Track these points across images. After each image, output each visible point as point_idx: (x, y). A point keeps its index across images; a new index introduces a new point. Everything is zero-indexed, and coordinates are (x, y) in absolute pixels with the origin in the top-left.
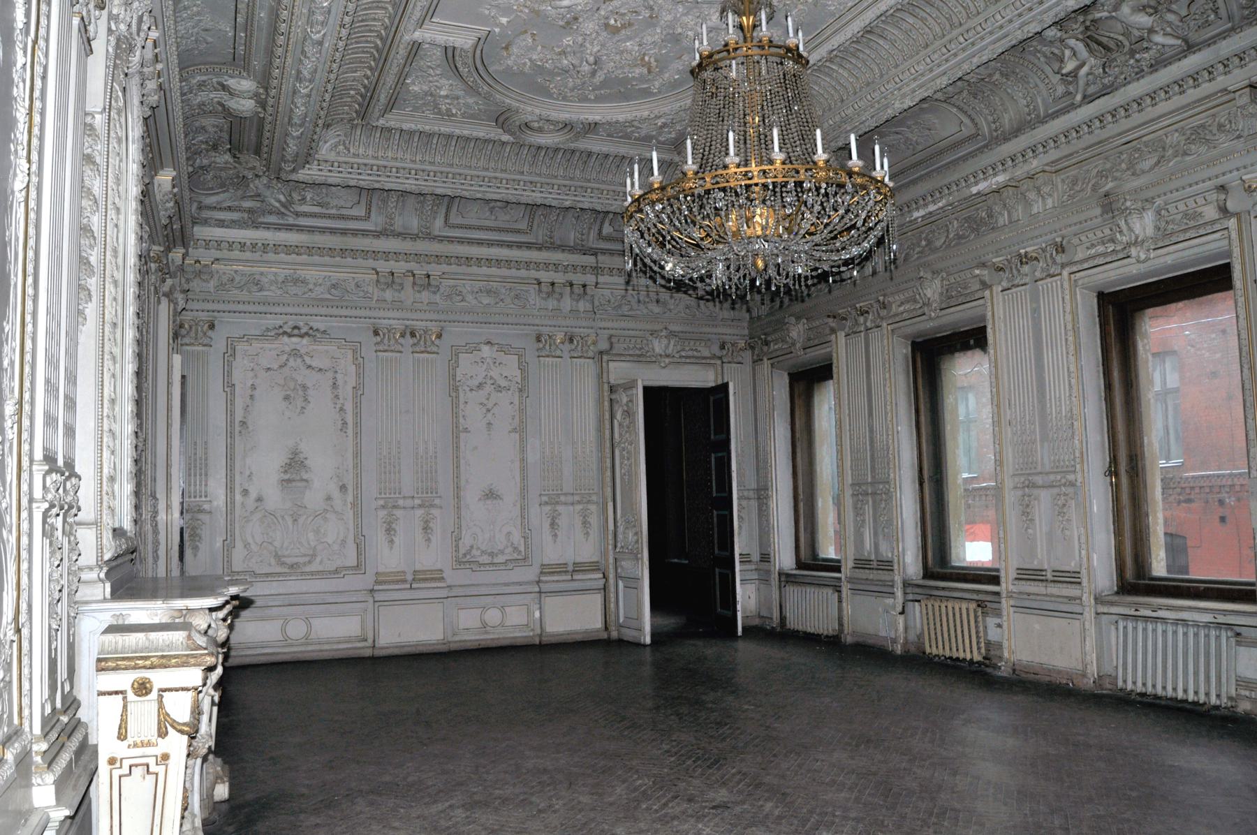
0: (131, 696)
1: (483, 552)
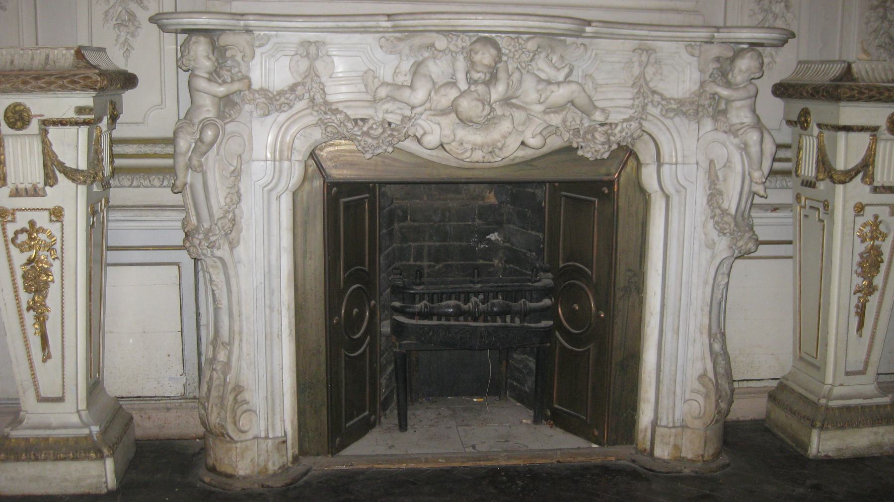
0: (884, 133)
1: (483, 109)
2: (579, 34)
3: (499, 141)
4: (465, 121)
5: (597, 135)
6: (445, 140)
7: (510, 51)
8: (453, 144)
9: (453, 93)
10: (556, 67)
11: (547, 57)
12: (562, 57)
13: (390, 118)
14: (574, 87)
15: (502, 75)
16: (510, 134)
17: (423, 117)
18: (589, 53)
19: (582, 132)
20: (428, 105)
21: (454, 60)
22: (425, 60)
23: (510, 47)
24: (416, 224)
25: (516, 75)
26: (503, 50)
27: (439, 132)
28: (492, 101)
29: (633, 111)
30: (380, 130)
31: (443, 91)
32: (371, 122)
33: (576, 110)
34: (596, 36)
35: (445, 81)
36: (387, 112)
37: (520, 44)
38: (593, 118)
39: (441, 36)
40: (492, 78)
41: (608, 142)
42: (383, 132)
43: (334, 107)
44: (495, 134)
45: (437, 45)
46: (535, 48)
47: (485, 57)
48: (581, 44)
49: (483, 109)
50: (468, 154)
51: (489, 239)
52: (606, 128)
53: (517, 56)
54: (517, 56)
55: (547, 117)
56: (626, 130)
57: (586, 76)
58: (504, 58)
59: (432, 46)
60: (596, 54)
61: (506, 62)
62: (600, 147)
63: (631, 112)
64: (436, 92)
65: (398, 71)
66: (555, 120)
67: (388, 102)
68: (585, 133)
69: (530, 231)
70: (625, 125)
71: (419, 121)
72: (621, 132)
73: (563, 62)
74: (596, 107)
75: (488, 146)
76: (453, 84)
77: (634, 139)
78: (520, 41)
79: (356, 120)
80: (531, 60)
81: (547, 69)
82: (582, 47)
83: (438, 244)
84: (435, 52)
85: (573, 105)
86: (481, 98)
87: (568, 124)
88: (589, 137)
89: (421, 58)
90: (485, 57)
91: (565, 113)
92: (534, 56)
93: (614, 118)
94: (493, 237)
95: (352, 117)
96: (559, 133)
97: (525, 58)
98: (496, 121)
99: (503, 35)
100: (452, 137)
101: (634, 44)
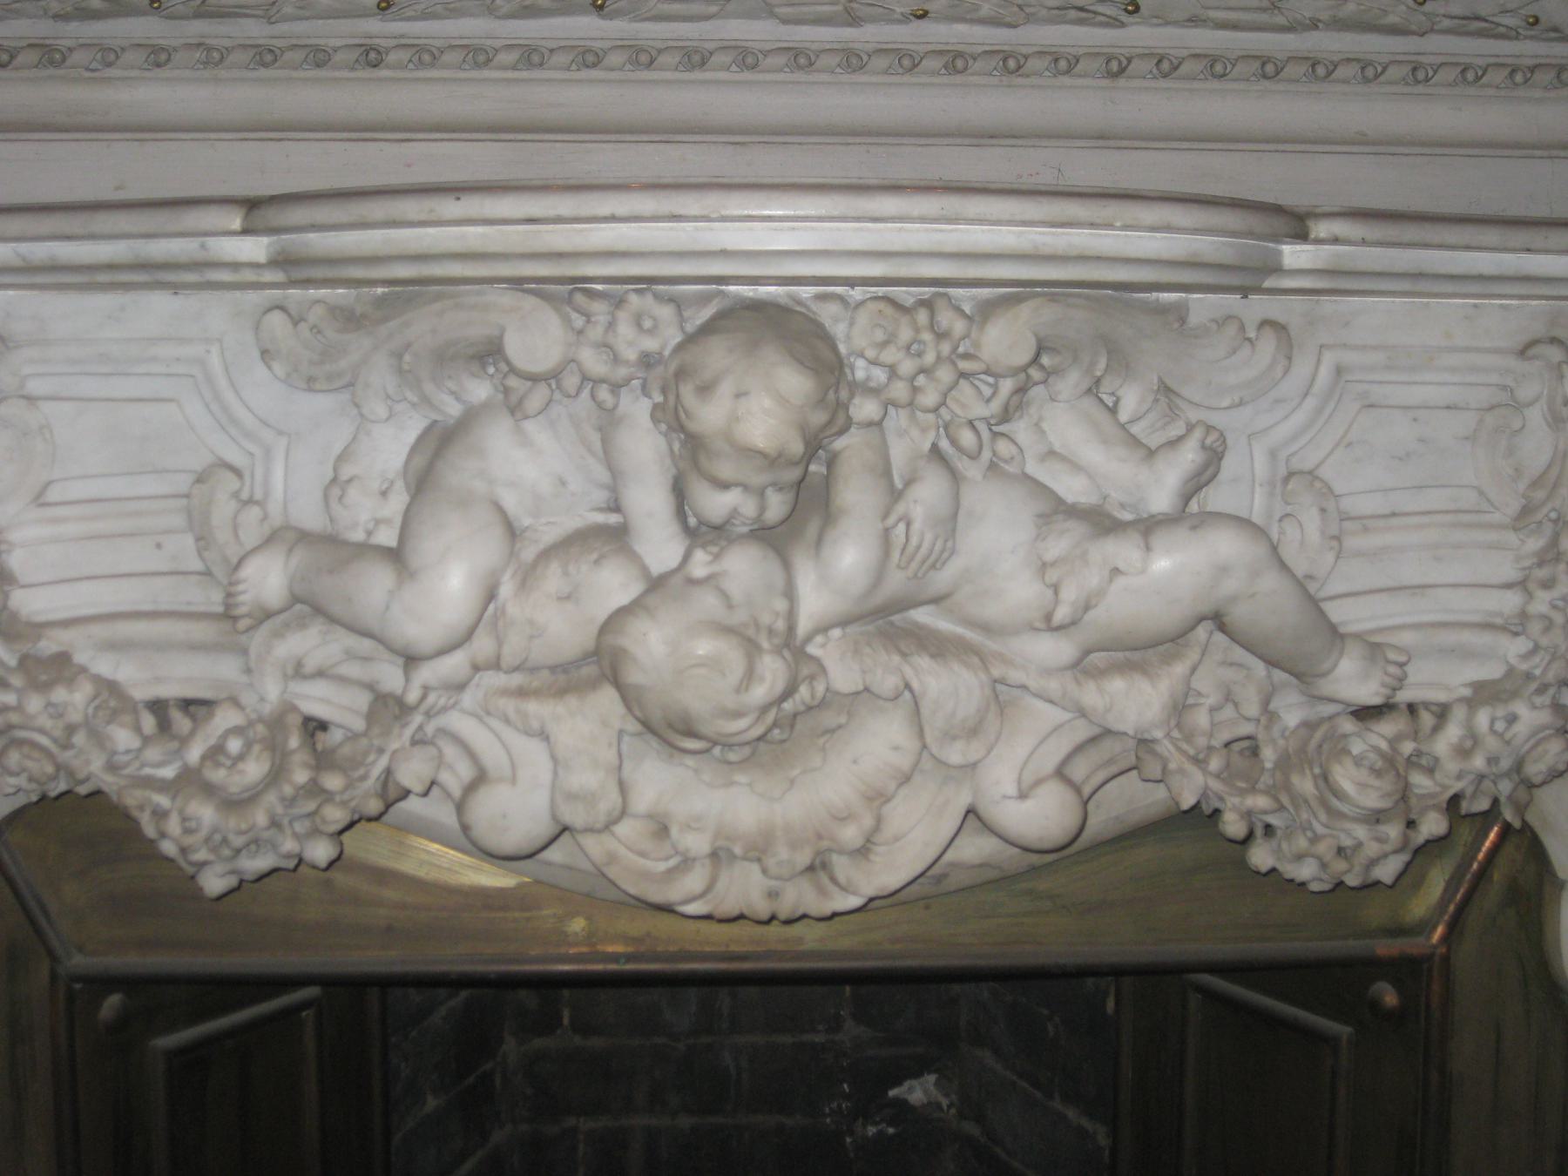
1: (750, 676)
2: (1251, 277)
3: (844, 818)
4: (671, 731)
5: (1346, 777)
6: (575, 815)
7: (892, 371)
8: (624, 829)
9: (613, 586)
10: (1135, 442)
11: (1093, 390)
12: (1166, 389)
13: (317, 699)
14: (1226, 545)
15: (856, 495)
16: (906, 779)
17: (468, 699)
18: (1302, 368)
19: (1269, 755)
20: (483, 645)
21: (609, 422)
22: (471, 417)
23: (890, 355)
24: (596, 1042)
25: (929, 494)
26: (861, 370)
27: (545, 776)
28: (804, 625)
29: (1520, 645)
30: (254, 769)
31: (553, 579)
32: (225, 719)
33: (1239, 654)
34: (1339, 281)
35: (571, 523)
36: (298, 671)
37: (941, 336)
38: (1327, 687)
39: (530, 302)
40: (804, 501)
41: (1404, 808)
42: (276, 775)
43: (48, 646)
44: (827, 786)
45: (514, 346)
46: (1023, 356)
47: (759, 406)
48: (1265, 323)
49: (750, 676)
50: (694, 881)
51: (901, 1104)
52: (1388, 727)
53: (929, 398)
54: (929, 398)
55: (1091, 695)
56: (1492, 743)
57: (1293, 478)
58: (865, 409)
59: (489, 353)
60: (1339, 371)
61: (878, 424)
62: (1361, 832)
63: (1514, 648)
64: (527, 578)
65: (347, 471)
66: (1136, 702)
67: (301, 623)
68: (1285, 764)
69: (1057, 1104)
70: (1482, 719)
71: (458, 722)
72: (1463, 752)
73: (1172, 413)
74: (1336, 636)
75: (794, 845)
76: (613, 537)
77: (1531, 786)
78: (945, 318)
79: (158, 707)
80: (1006, 416)
81: (1093, 454)
82: (1268, 345)
83: (685, 1122)
84: (513, 382)
85: (1222, 628)
86: (739, 617)
87: (1201, 719)
88: (1305, 784)
89: (454, 409)
90: (759, 406)
91: (1180, 669)
92: (1021, 390)
93: (1432, 680)
94: (918, 1091)
95: (141, 694)
96: (1153, 769)
97: (972, 403)
98: (829, 718)
99: (857, 293)
100: (611, 799)
101: (1527, 316)
